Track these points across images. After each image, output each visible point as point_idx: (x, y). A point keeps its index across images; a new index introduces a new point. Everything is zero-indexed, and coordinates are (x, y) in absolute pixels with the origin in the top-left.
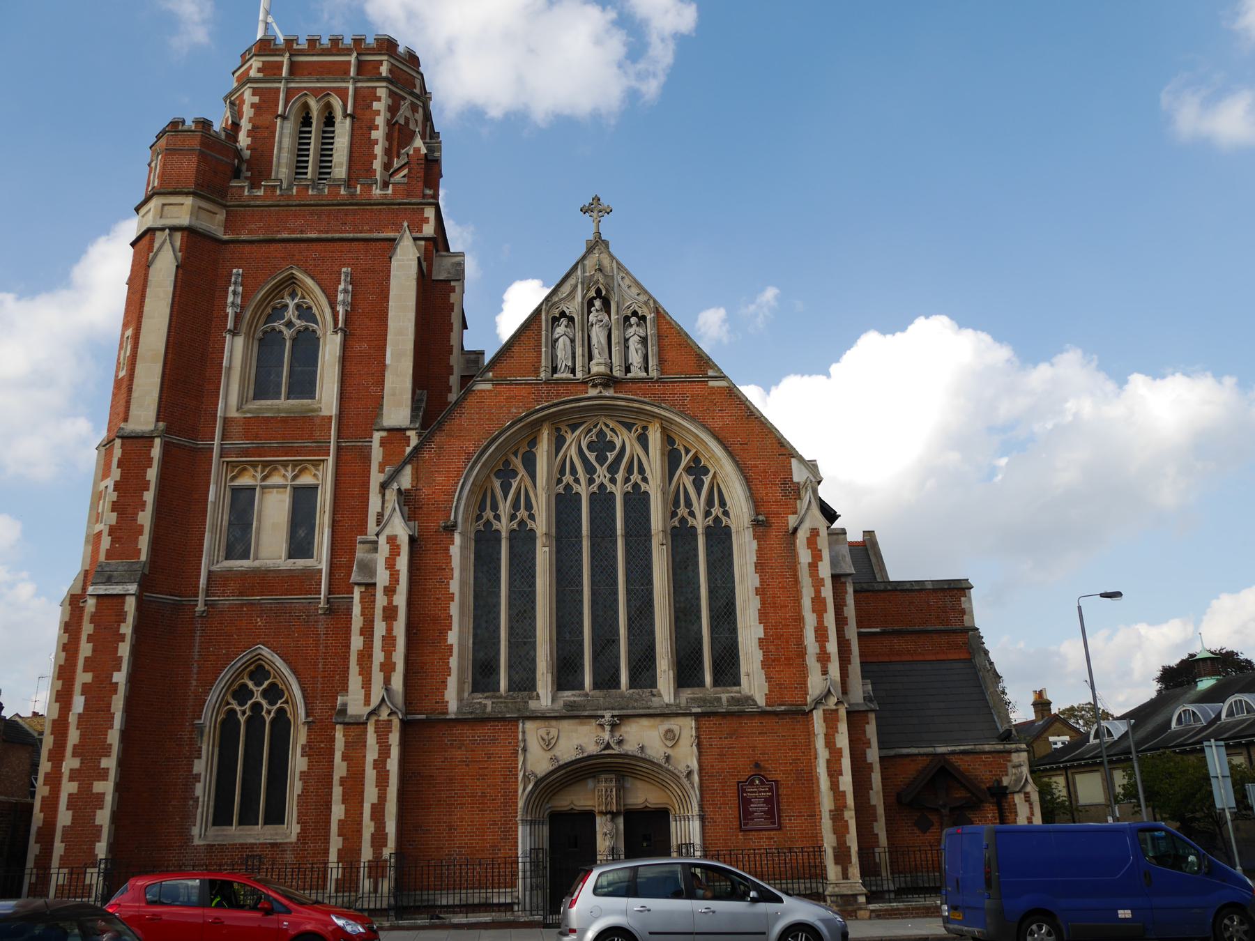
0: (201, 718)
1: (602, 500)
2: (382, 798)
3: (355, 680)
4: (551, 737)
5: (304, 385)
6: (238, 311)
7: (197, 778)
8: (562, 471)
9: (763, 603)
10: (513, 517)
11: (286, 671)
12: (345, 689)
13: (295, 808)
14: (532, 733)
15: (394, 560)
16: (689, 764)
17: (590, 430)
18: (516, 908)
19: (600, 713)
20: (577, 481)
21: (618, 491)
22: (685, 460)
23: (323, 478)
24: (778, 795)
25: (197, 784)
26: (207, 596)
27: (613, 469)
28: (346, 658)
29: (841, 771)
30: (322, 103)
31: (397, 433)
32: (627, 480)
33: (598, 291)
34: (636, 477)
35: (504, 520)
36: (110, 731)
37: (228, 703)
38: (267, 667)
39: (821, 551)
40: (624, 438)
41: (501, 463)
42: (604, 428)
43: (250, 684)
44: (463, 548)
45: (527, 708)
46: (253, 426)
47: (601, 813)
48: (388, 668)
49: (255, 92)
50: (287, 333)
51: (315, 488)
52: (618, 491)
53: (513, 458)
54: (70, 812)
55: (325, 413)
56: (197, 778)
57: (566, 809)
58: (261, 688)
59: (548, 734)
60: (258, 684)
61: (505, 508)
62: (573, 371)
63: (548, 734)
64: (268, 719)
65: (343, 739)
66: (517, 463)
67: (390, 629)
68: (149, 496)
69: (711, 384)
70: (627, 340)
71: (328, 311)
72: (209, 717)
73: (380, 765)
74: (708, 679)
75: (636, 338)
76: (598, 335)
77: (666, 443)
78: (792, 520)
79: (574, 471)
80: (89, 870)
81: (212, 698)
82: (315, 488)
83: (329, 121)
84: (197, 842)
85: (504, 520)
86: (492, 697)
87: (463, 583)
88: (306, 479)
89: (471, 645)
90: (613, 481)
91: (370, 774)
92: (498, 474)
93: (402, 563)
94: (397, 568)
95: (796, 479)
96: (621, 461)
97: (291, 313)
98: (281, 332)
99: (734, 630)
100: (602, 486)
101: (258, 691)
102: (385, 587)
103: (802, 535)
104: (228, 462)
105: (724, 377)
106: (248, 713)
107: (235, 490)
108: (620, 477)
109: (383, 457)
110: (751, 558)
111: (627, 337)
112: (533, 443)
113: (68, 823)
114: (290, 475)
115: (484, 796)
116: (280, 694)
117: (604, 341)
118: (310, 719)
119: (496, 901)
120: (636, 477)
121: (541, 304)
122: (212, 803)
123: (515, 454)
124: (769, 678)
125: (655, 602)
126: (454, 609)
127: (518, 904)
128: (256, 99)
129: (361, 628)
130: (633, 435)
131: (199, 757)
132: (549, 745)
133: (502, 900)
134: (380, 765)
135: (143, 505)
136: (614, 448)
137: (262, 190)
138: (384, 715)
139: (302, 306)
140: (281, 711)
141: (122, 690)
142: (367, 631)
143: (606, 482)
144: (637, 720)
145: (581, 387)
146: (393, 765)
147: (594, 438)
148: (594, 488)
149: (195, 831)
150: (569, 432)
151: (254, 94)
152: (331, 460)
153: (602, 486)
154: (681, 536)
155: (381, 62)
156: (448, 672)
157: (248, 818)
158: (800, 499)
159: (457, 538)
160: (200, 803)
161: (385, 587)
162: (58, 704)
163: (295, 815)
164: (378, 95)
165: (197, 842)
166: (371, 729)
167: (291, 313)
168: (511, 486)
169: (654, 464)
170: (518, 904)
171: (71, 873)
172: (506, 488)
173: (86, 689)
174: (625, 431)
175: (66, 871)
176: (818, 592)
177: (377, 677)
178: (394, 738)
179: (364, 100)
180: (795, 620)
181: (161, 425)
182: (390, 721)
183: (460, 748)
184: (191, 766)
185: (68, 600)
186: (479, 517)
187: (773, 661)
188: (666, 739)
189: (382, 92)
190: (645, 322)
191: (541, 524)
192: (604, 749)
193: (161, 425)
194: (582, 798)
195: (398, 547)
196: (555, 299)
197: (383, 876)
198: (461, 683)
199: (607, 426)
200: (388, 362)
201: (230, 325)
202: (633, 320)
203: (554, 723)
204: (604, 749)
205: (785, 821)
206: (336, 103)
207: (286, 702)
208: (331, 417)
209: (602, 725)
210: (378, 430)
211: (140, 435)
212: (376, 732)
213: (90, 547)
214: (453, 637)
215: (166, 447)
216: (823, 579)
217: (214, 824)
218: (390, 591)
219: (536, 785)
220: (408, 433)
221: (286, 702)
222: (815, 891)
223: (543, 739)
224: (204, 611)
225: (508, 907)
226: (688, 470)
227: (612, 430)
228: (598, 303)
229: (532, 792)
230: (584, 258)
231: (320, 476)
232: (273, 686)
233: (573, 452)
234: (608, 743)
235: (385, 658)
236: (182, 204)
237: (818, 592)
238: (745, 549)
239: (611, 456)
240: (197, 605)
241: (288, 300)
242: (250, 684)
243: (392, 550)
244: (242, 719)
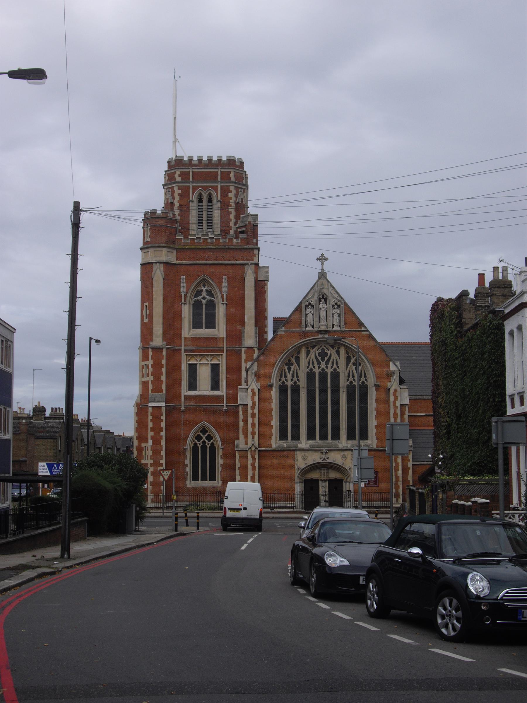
0: (186, 446)
1: (323, 375)
2: (254, 474)
3: (241, 436)
4: (305, 456)
5: (211, 324)
6: (185, 294)
7: (186, 466)
8: (309, 364)
9: (377, 413)
10: (292, 380)
11: (213, 430)
12: (238, 438)
13: (220, 476)
14: (299, 455)
15: (254, 397)
16: (350, 466)
17: (319, 348)
18: (295, 508)
19: (321, 449)
20: (314, 367)
21: (329, 371)
22: (353, 360)
23: (222, 362)
24: (378, 476)
25: (187, 468)
26: (184, 404)
27: (327, 363)
28: (238, 429)
29: (398, 470)
30: (207, 193)
31: (250, 349)
32: (332, 367)
33: (323, 296)
34: (335, 366)
35: (289, 381)
36: (162, 451)
37: (194, 441)
38: (206, 429)
39: (397, 397)
40: (332, 352)
41: (287, 360)
42: (324, 348)
43: (201, 435)
44: (276, 391)
45: (298, 447)
46: (195, 340)
47: (321, 480)
48: (253, 433)
49: (179, 188)
50: (204, 302)
51: (218, 364)
52: (329, 371)
53: (292, 359)
54: (152, 477)
55: (221, 336)
56: (186, 466)
57: (310, 478)
58: (205, 436)
59: (305, 455)
60: (204, 434)
61: (289, 377)
62: (313, 327)
63: (305, 455)
64: (208, 446)
65: (239, 455)
66: (293, 360)
67: (253, 421)
68: (164, 370)
69: (363, 333)
70: (333, 314)
71: (219, 294)
72: (189, 445)
73: (253, 464)
74: (208, 479)
75: (336, 314)
76: (323, 314)
77: (346, 354)
78: (389, 384)
79: (313, 364)
80: (160, 495)
81: (189, 439)
82: (218, 364)
83: (210, 200)
84: (188, 486)
85: (289, 381)
86: (286, 442)
87: (276, 404)
88: (215, 361)
89: (278, 425)
90: (327, 367)
91: (250, 467)
92: (286, 364)
93: (256, 399)
94: (255, 400)
95: (391, 369)
96: (330, 360)
97: (204, 294)
98: (201, 301)
99: (367, 421)
100: (323, 369)
101: (204, 437)
102: (251, 407)
103: (392, 391)
104: (186, 355)
105: (368, 331)
106: (206, 444)
107: (190, 365)
108: (330, 365)
109: (246, 358)
110: (374, 397)
111: (333, 313)
112: (299, 353)
113: (152, 480)
114: (209, 359)
115: (284, 474)
116: (212, 438)
117: (325, 315)
118: (223, 447)
119: (289, 506)
120: (335, 366)
121: (302, 300)
122: (192, 474)
123: (292, 357)
124: (377, 439)
125: (340, 411)
126: (273, 413)
127: (295, 507)
128: (180, 191)
129: (243, 419)
130: (334, 351)
131: (187, 459)
132: (304, 459)
133: (291, 506)
134: (253, 464)
135: (162, 373)
136: (328, 355)
137: (189, 240)
138: (253, 449)
139: (208, 290)
140: (212, 444)
141: (164, 438)
142: (246, 420)
143: (324, 368)
144: (334, 451)
145: (316, 334)
146: (257, 464)
147: (320, 351)
148: (320, 370)
149: (187, 482)
150: (312, 349)
151: (179, 189)
152: (224, 354)
153: (323, 369)
154: (351, 389)
155: (230, 172)
156: (272, 434)
157: (204, 479)
158: (392, 377)
159: (274, 389)
160: (188, 474)
161: (251, 407)
162: (137, 441)
163: (220, 478)
164: (230, 189)
165: (188, 486)
166: (249, 453)
167: (204, 294)
168: (291, 369)
169: (342, 361)
170: (295, 507)
171: (155, 495)
172: (289, 369)
173: (152, 438)
174: (332, 349)
175: (153, 495)
176: (395, 411)
177: (250, 436)
178: (257, 456)
179: (225, 191)
180: (388, 419)
181: (165, 343)
182: (255, 451)
183: (276, 459)
184: (184, 462)
185: (136, 404)
186: (280, 380)
187: (379, 433)
188: (343, 458)
189: (232, 188)
190: (340, 307)
191: (303, 383)
192: (323, 460)
193: (165, 343)
194: (314, 475)
195: (255, 393)
196: (307, 298)
197: (370, 512)
198: (276, 437)
199: (325, 347)
200: (246, 320)
201: (183, 301)
202: (336, 306)
203: (306, 451)
204: (323, 460)
205: (380, 484)
206: (214, 194)
207: (214, 441)
208: (223, 337)
209: (322, 453)
210: (243, 347)
211: (158, 347)
212: (251, 454)
213: (141, 386)
214: (273, 423)
215: (167, 349)
216: (397, 406)
217: (193, 481)
218: (253, 408)
219: (301, 471)
220: (254, 349)
221: (214, 441)
222: (387, 505)
223: (303, 457)
224: (184, 410)
225: (292, 507)
226: (354, 364)
227: (327, 348)
228: (323, 300)
229: (299, 473)
230: (317, 281)
231: (220, 360)
232: (209, 435)
233: (313, 356)
234: (324, 458)
235: (252, 430)
236: (162, 251)
237: (395, 411)
238: (372, 394)
239: (326, 358)
240: (181, 407)
241: (203, 288)
242: (201, 435)
243: (253, 394)
244: (200, 446)
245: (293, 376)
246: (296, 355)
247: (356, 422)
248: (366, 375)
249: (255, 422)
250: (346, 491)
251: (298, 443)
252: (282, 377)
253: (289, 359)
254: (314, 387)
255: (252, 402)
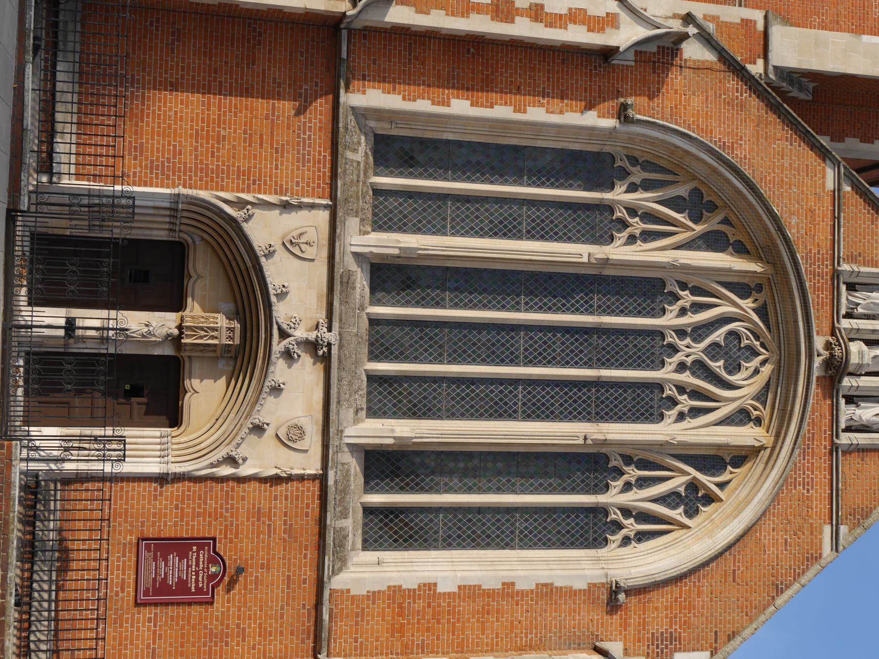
9: (490, 594)
19: (336, 325)
27: (700, 368)
34: (686, 402)
42: (761, 358)
53: (719, 218)
69: (827, 529)
77: (736, 453)
79: (698, 307)
90: (682, 367)
92: (697, 193)
115: (220, 139)
123: (726, 221)
125: (496, 422)
132: (291, 245)
136: (730, 373)
148: (671, 338)
172: (674, 203)
186: (634, 161)
195: (601, 30)
199: (764, 363)
200: (866, 38)
210: (766, 17)
226: (693, 486)
233: (725, 309)
234: (289, 336)
239: (717, 366)
245: (649, 216)
246: (732, 235)
247: (446, 492)
248: (648, 539)
249: (474, 16)
250: (122, 440)
251: (362, 220)
252: (644, 169)
253: (717, 207)
254: (599, 307)
255: (564, 12)
